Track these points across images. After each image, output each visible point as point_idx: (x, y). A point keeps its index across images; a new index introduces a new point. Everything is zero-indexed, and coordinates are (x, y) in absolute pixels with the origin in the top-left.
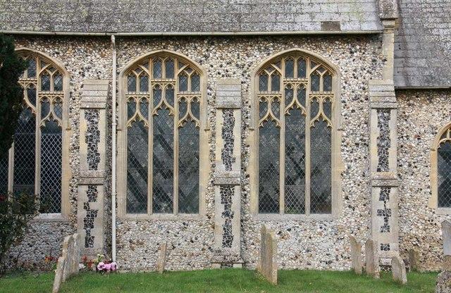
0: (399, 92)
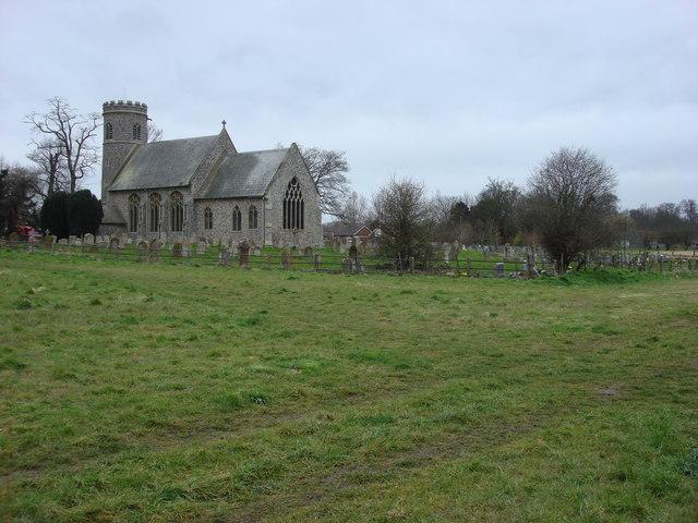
0: (195, 200)
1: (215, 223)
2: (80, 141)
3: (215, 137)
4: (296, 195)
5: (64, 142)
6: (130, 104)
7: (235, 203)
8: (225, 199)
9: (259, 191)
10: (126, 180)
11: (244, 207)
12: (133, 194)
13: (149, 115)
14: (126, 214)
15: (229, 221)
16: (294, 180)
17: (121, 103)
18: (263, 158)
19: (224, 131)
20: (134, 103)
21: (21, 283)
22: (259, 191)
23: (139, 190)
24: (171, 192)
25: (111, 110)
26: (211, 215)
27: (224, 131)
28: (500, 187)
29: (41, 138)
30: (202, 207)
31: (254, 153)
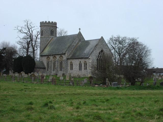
1: (74, 67)
2: (36, 36)
3: (76, 34)
4: (101, 57)
5: (31, 37)
6: (49, 22)
7: (80, 60)
8: (78, 58)
9: (87, 55)
10: (46, 51)
11: (83, 61)
12: (48, 56)
13: (57, 26)
14: (46, 64)
15: (78, 67)
16: (102, 51)
17: (46, 22)
18: (91, 43)
19: (80, 32)
20: (51, 22)
21: (124, 113)
22: (87, 55)
23: (50, 55)
24: (59, 56)
25: (43, 24)
26: (72, 64)
27: (80, 32)
28: (9, 44)
29: (23, 35)
30: (69, 61)
31: (89, 40)
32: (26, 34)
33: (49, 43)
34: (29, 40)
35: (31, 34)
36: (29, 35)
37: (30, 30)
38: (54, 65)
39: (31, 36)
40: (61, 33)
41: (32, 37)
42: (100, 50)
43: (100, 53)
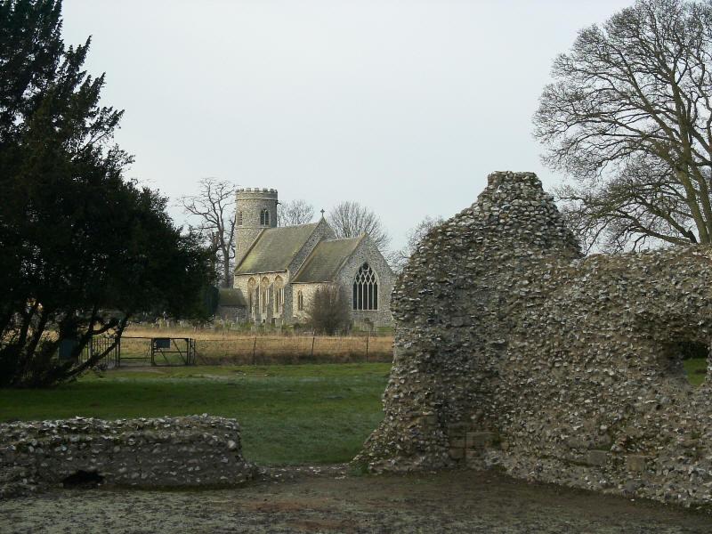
16: (366, 266)
19: (323, 219)
27: (323, 219)
32: (206, 217)
33: (255, 243)
34: (216, 230)
35: (219, 215)
36: (212, 219)
37: (217, 205)
38: (376, 298)
39: (218, 221)
40: (295, 213)
41: (220, 223)
42: (362, 264)
43: (360, 271)
